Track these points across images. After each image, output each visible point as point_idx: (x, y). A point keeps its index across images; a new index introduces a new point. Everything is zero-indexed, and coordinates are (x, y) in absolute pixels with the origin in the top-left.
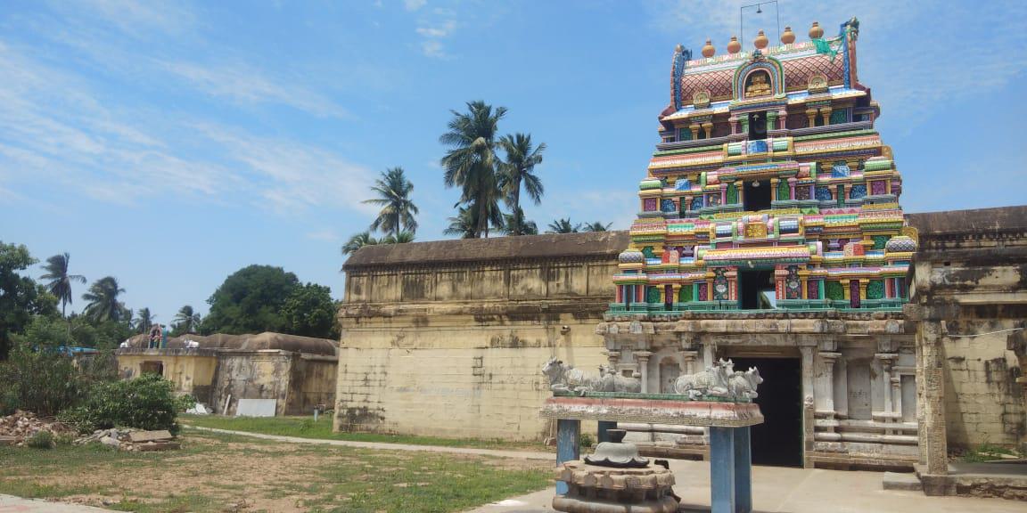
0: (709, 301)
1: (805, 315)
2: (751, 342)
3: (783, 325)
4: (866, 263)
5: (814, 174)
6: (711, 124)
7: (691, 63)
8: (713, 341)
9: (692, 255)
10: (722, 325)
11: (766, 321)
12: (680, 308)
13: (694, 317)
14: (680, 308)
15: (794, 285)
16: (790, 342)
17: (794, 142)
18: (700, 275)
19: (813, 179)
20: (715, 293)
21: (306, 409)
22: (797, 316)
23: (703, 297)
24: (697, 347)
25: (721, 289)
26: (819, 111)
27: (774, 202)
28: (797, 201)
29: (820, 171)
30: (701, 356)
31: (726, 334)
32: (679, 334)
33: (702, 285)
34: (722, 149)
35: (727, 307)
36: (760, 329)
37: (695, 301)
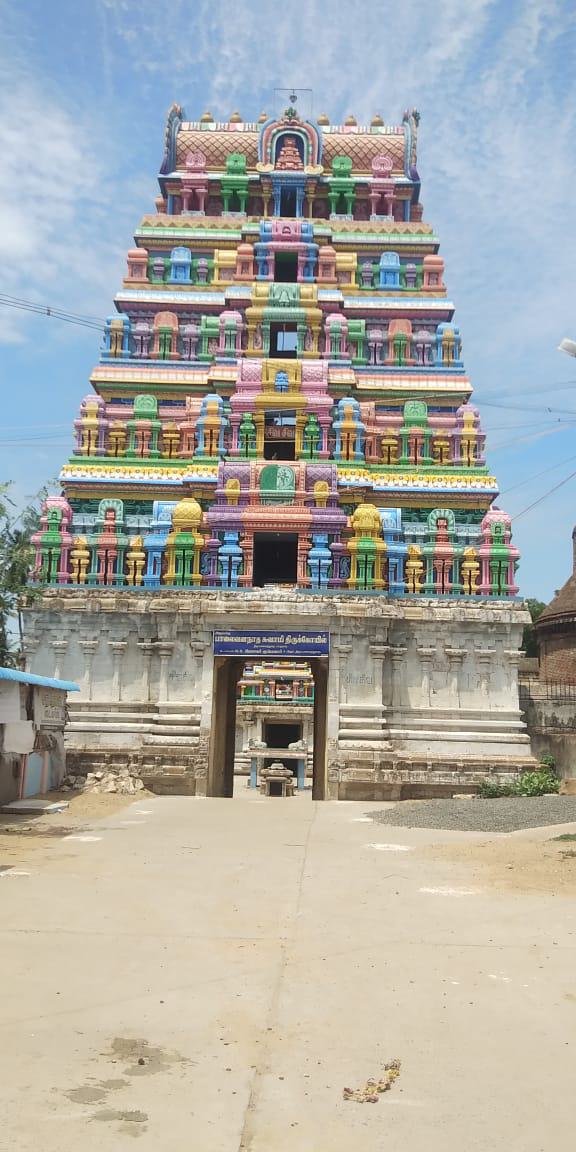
0: (261, 696)
1: (306, 705)
2: (280, 717)
3: (296, 710)
4: (428, 425)
5: (363, 330)
6: (206, 191)
7: (185, 126)
8: (262, 716)
9: (252, 670)
10: (267, 709)
11: (288, 707)
12: (245, 699)
13: (253, 704)
14: (245, 699)
15: (301, 690)
16: (299, 718)
17: (330, 365)
18: (256, 682)
19: (362, 333)
20: (264, 692)
21: (190, 783)
22: (302, 705)
23: (258, 694)
24: (254, 719)
25: (267, 690)
26: (383, 197)
27: (300, 277)
28: (355, 195)
30: (255, 724)
32: (245, 713)
33: (257, 687)
35: (270, 699)
36: (286, 711)
37: (253, 696)
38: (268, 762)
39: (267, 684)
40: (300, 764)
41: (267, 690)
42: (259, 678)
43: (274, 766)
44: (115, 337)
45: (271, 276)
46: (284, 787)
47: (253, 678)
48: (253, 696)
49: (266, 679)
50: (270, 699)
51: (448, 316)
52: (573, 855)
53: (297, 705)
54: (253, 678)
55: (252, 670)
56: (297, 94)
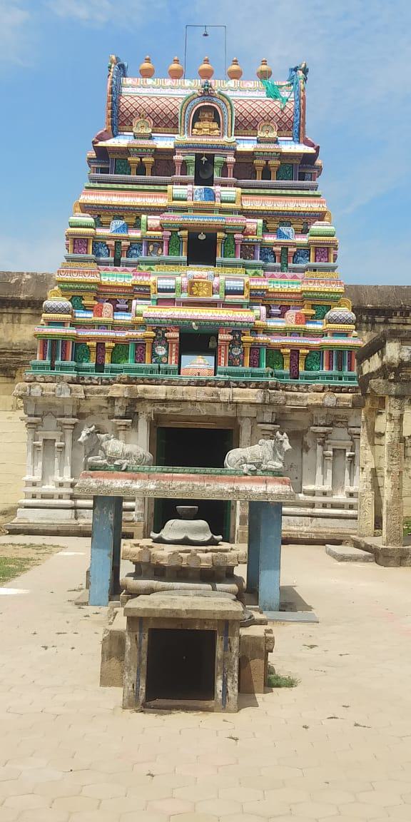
0: (147, 364)
2: (189, 411)
7: (128, 81)
8: (149, 408)
10: (161, 391)
12: (113, 370)
13: (130, 381)
14: (113, 370)
15: (237, 352)
16: (230, 412)
18: (138, 334)
20: (154, 355)
22: (238, 385)
23: (142, 360)
24: (131, 414)
25: (161, 351)
29: (266, 230)
30: (135, 425)
31: (165, 402)
32: (112, 400)
33: (140, 345)
34: (166, 191)
35: (167, 371)
36: (201, 397)
38: (165, 510)
39: (160, 339)
40: (131, 614)
41: (161, 351)
42: (143, 326)
43: (175, 528)
44: (78, 242)
45: (184, 257)
46: (226, 653)
47: (132, 327)
48: (130, 363)
49: (160, 328)
50: (167, 371)
51: (320, 216)
52: (4, 513)
53: (227, 384)
54: (132, 327)
55: (128, 310)
56: (209, 30)
